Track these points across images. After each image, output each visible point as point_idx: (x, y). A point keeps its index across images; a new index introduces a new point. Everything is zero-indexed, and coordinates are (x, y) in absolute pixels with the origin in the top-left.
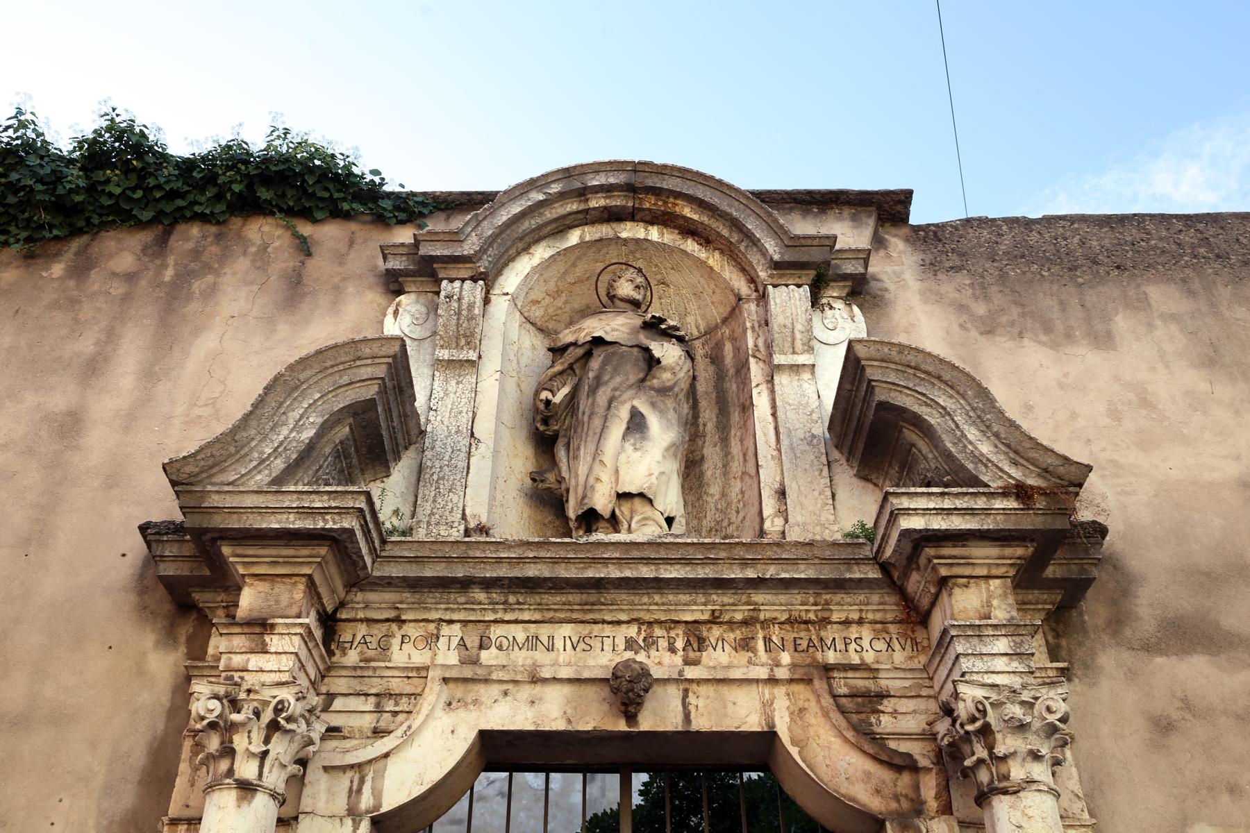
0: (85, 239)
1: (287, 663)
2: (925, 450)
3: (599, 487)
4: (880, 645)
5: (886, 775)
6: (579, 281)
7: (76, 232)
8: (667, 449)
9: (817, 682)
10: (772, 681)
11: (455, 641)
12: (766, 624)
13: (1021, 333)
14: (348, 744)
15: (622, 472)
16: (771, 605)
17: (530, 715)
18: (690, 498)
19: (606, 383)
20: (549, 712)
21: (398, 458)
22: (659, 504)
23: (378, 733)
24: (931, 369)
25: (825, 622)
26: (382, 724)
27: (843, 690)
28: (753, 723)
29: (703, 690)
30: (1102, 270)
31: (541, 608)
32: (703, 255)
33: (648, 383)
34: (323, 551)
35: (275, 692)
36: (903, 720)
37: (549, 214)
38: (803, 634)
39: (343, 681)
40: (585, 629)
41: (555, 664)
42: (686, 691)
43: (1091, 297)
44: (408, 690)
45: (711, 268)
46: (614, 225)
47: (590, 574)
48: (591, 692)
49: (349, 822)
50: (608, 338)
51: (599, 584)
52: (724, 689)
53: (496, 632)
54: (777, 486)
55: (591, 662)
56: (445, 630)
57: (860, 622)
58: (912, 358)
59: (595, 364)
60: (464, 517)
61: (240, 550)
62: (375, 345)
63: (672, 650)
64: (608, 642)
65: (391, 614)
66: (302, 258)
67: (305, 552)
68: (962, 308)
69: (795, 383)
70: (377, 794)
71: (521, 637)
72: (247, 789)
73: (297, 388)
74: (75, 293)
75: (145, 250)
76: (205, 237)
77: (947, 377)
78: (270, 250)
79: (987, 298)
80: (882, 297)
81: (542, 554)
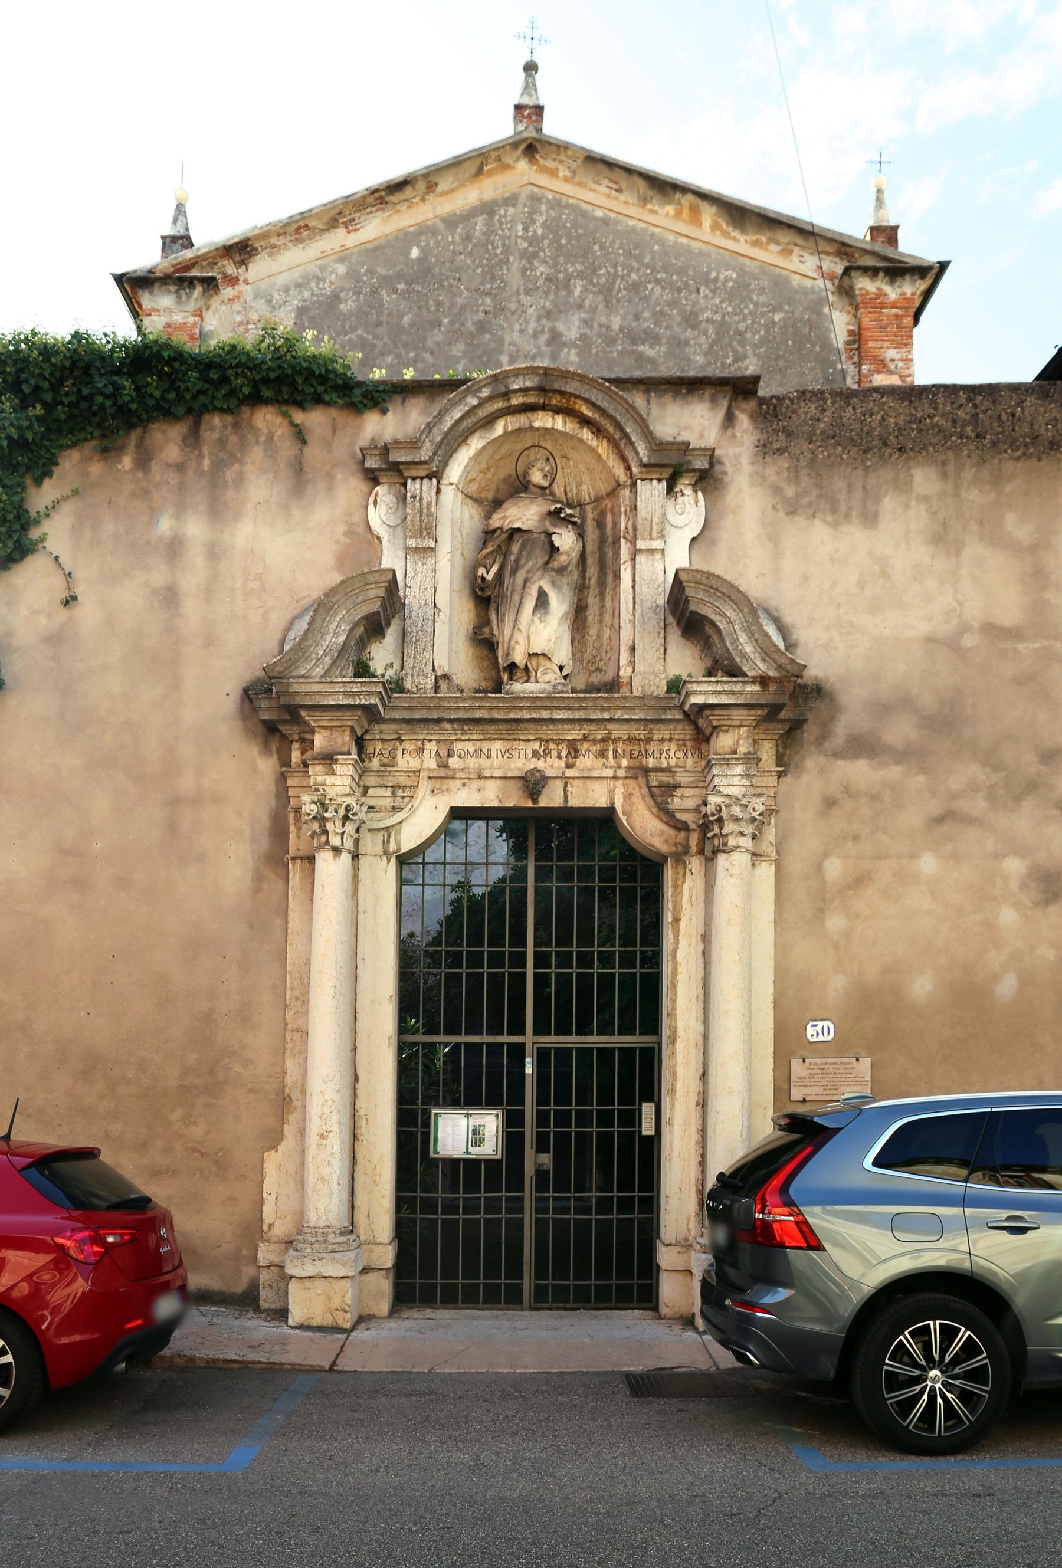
0: (138, 431)
1: (347, 781)
2: (717, 642)
3: (517, 647)
4: (680, 755)
5: (672, 832)
6: (503, 458)
7: (131, 427)
8: (561, 618)
9: (640, 779)
10: (615, 778)
11: (434, 753)
12: (615, 741)
13: (815, 513)
14: (379, 815)
15: (532, 639)
16: (618, 731)
17: (478, 798)
18: (577, 636)
19: (523, 567)
20: (489, 796)
21: (388, 625)
22: (555, 660)
23: (395, 809)
24: (725, 591)
25: (649, 740)
26: (396, 804)
27: (655, 783)
28: (602, 802)
29: (576, 782)
30: (888, 451)
31: (483, 732)
32: (594, 443)
33: (550, 565)
34: (359, 713)
35: (344, 799)
36: (683, 802)
37: (481, 413)
38: (636, 747)
39: (372, 779)
40: (508, 744)
41: (491, 767)
42: (566, 783)
43: (873, 480)
44: (409, 783)
45: (600, 456)
46: (529, 414)
47: (512, 716)
48: (513, 784)
49: (385, 858)
50: (524, 528)
51: (517, 721)
52: (588, 782)
53: (457, 746)
54: (630, 643)
55: (512, 766)
56: (427, 745)
57: (670, 740)
58: (714, 583)
59: (515, 548)
60: (434, 670)
61: (311, 713)
62: (377, 575)
63: (559, 757)
64: (522, 752)
65: (396, 736)
66: (300, 445)
67: (349, 714)
68: (777, 490)
69: (650, 562)
70: (398, 843)
71: (471, 751)
72: (337, 850)
73: (332, 608)
74: (145, 484)
75: (184, 439)
76: (225, 427)
77: (734, 597)
78: (275, 438)
79: (797, 481)
80: (721, 480)
81: (484, 704)
